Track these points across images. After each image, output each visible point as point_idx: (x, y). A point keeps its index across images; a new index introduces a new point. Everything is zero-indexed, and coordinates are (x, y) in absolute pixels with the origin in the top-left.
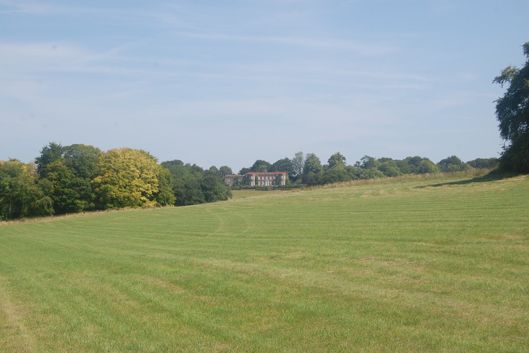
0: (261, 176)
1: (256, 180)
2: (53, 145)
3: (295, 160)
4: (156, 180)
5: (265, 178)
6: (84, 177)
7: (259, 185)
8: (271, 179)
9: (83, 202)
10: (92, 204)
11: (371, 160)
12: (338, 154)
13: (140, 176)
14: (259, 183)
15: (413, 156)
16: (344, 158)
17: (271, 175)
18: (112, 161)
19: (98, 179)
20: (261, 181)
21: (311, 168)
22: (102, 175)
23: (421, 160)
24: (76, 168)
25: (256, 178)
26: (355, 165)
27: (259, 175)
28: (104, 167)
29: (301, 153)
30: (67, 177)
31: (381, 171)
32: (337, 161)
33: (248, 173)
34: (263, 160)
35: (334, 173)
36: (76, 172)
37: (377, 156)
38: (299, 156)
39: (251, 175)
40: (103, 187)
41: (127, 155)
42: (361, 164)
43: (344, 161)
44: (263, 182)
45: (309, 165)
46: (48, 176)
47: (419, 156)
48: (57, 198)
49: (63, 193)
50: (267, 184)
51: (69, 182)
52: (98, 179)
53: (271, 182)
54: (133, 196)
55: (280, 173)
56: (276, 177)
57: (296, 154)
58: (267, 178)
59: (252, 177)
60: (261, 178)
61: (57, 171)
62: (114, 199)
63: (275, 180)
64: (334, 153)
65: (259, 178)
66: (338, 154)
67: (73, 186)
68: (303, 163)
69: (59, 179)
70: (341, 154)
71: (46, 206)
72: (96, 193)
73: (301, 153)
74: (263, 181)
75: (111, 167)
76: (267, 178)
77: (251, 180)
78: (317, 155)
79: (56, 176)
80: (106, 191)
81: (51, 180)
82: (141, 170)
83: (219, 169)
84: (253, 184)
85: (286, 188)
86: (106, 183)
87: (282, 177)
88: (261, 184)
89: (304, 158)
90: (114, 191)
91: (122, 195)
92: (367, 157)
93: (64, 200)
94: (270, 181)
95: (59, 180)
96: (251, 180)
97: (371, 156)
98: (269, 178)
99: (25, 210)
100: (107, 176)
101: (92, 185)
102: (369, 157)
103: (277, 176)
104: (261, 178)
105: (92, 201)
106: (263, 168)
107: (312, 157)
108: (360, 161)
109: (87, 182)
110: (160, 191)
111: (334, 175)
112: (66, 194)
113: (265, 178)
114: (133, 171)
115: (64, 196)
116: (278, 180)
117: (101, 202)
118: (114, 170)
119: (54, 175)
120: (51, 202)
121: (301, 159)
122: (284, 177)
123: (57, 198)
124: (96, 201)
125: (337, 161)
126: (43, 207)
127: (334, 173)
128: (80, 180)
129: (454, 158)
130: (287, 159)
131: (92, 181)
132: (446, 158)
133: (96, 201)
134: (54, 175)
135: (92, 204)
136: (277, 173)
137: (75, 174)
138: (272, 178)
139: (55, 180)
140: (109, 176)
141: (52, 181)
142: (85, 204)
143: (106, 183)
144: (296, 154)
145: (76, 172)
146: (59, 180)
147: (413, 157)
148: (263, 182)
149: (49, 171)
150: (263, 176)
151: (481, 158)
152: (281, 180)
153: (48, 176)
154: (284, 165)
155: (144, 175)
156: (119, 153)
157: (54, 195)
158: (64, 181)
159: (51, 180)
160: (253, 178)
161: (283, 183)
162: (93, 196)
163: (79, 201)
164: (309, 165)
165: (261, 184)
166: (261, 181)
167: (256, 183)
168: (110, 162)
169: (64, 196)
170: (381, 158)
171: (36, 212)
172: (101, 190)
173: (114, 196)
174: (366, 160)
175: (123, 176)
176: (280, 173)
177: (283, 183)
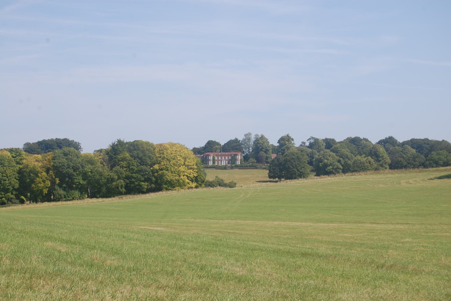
0: (218, 156)
1: (214, 160)
2: (119, 141)
3: (244, 140)
4: (196, 167)
5: (222, 158)
6: (146, 165)
7: (216, 164)
8: (227, 159)
9: (146, 184)
10: (153, 185)
11: (316, 140)
12: (288, 135)
13: (184, 164)
14: (216, 162)
15: (353, 137)
16: (293, 140)
17: (227, 155)
18: (165, 153)
19: (156, 167)
20: (218, 160)
21: (260, 148)
22: (159, 164)
23: (361, 140)
24: (140, 159)
25: (213, 157)
26: (301, 145)
27: (216, 156)
28: (160, 157)
29: (250, 134)
30: (134, 165)
31: (333, 152)
32: (287, 142)
33: (207, 154)
34: (214, 140)
35: (293, 155)
36: (139, 161)
37: (321, 136)
38: (248, 136)
39: (209, 155)
40: (160, 172)
41: (174, 149)
42: (307, 144)
43: (293, 142)
44: (220, 162)
45: (259, 145)
46: (120, 164)
47: (358, 136)
48: (128, 181)
49: (133, 177)
50: (224, 163)
51: (136, 169)
52: (156, 167)
53: (227, 162)
54: (181, 179)
55: (235, 153)
56: (232, 157)
57: (245, 135)
58: (223, 157)
59: (210, 157)
60: (218, 158)
61: (126, 161)
62: (168, 181)
63: (230, 160)
64: (284, 134)
65: (216, 158)
66: (288, 135)
67: (139, 171)
68: (252, 143)
69: (128, 167)
70: (290, 135)
71: (120, 187)
72: (155, 177)
73: (250, 134)
74: (220, 160)
75: (165, 157)
76: (223, 157)
77: (209, 160)
78: (266, 136)
79: (126, 164)
80: (162, 176)
81: (122, 167)
82: (185, 159)
83: (277, 145)
84: (211, 163)
85: (240, 167)
86: (162, 170)
87: (237, 157)
88: (218, 163)
89: (253, 139)
90: (169, 176)
91: (174, 179)
92: (312, 138)
93: (133, 183)
94: (226, 160)
95: (129, 168)
96: (209, 160)
97: (317, 137)
98: (225, 158)
99: (104, 190)
100: (163, 164)
101: (152, 171)
102: (314, 138)
103: (233, 155)
104: (218, 158)
105: (152, 183)
106: (217, 148)
107: (262, 137)
108: (305, 141)
109: (148, 168)
110: (198, 175)
111: (294, 157)
112: (134, 178)
113: (222, 158)
114: (179, 160)
115: (133, 180)
116: (233, 160)
117: (158, 184)
118: (167, 159)
119: (124, 164)
120: (123, 184)
121: (249, 139)
122: (239, 157)
123: (128, 181)
124: (156, 183)
125: (287, 142)
126: (118, 188)
127: (293, 155)
128: (144, 167)
129: (391, 138)
130: (236, 139)
131: (152, 168)
132: (383, 138)
133: (156, 183)
134: (124, 164)
135: (153, 185)
136: (233, 153)
137: (139, 163)
138: (228, 158)
139: (125, 167)
140: (164, 165)
141: (123, 168)
142: (148, 185)
143: (162, 170)
144: (245, 135)
145: (139, 161)
146: (129, 168)
147: (353, 137)
148: (220, 162)
149: (119, 161)
150: (220, 156)
151: (416, 138)
152: (236, 160)
153: (120, 164)
154: (233, 146)
155: (186, 163)
156: (168, 146)
157: (125, 178)
158: (132, 168)
159: (122, 167)
160: (211, 158)
161: (238, 163)
162: (154, 179)
163: (143, 183)
164: (259, 145)
165: (218, 163)
166: (218, 160)
167: (214, 163)
168: (163, 154)
169: (133, 180)
170: (324, 138)
171: (110, 192)
172: (158, 174)
173: (169, 179)
174: (312, 141)
175: (174, 164)
176: (235, 153)
177: (238, 163)
